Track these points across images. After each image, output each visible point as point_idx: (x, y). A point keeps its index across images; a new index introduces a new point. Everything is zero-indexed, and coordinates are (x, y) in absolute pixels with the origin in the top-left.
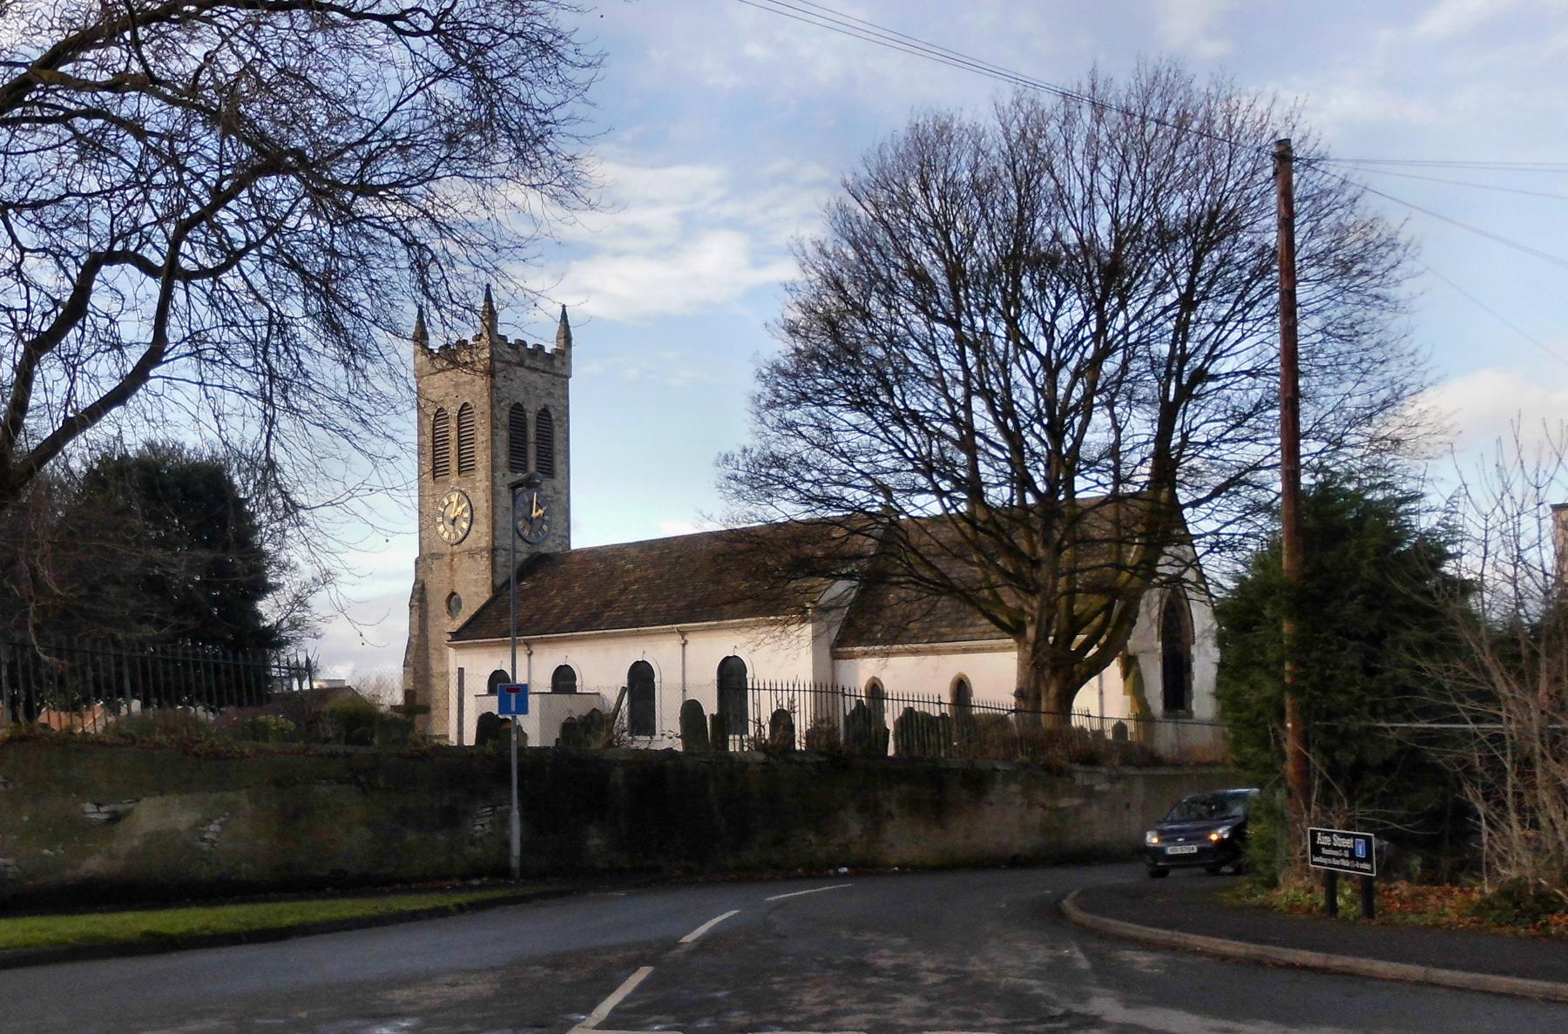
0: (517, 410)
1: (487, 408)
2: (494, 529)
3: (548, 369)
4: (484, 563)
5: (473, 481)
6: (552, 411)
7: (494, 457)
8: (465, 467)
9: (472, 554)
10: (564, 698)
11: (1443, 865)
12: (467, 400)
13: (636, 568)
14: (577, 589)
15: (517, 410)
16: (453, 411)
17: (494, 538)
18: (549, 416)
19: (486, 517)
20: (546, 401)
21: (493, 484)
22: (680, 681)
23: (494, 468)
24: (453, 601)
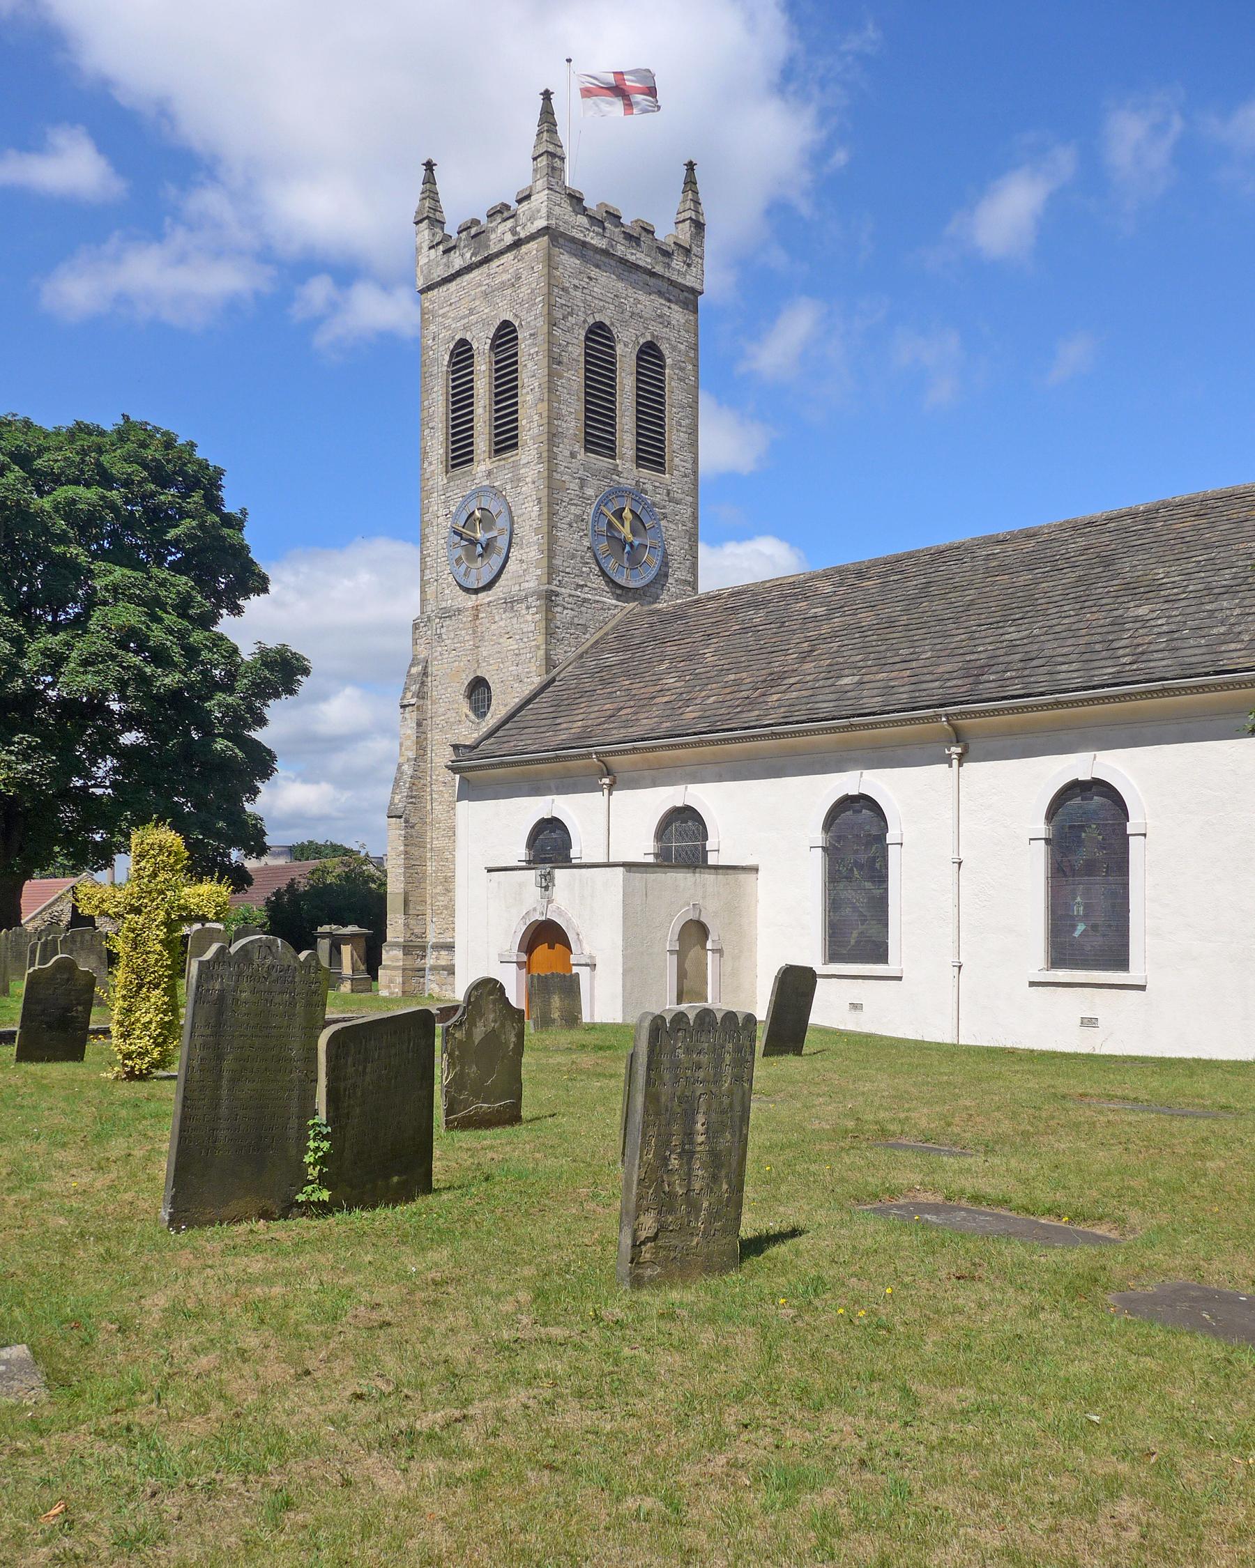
0: (599, 336)
1: (541, 324)
2: (551, 554)
3: (659, 269)
4: (530, 619)
5: (516, 466)
6: (664, 348)
7: (553, 417)
8: (506, 441)
9: (510, 603)
10: (683, 879)
11: (1079, 928)
12: (508, 316)
13: (831, 611)
14: (709, 658)
15: (599, 336)
16: (481, 344)
17: (551, 571)
18: (661, 357)
19: (537, 531)
20: (656, 328)
21: (551, 470)
22: (621, 868)
23: (553, 437)
24: (478, 690)
